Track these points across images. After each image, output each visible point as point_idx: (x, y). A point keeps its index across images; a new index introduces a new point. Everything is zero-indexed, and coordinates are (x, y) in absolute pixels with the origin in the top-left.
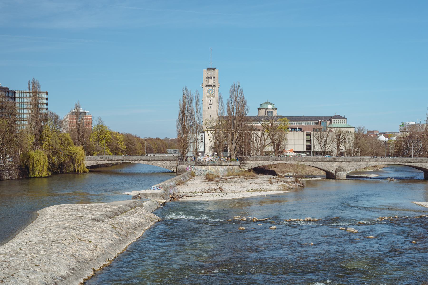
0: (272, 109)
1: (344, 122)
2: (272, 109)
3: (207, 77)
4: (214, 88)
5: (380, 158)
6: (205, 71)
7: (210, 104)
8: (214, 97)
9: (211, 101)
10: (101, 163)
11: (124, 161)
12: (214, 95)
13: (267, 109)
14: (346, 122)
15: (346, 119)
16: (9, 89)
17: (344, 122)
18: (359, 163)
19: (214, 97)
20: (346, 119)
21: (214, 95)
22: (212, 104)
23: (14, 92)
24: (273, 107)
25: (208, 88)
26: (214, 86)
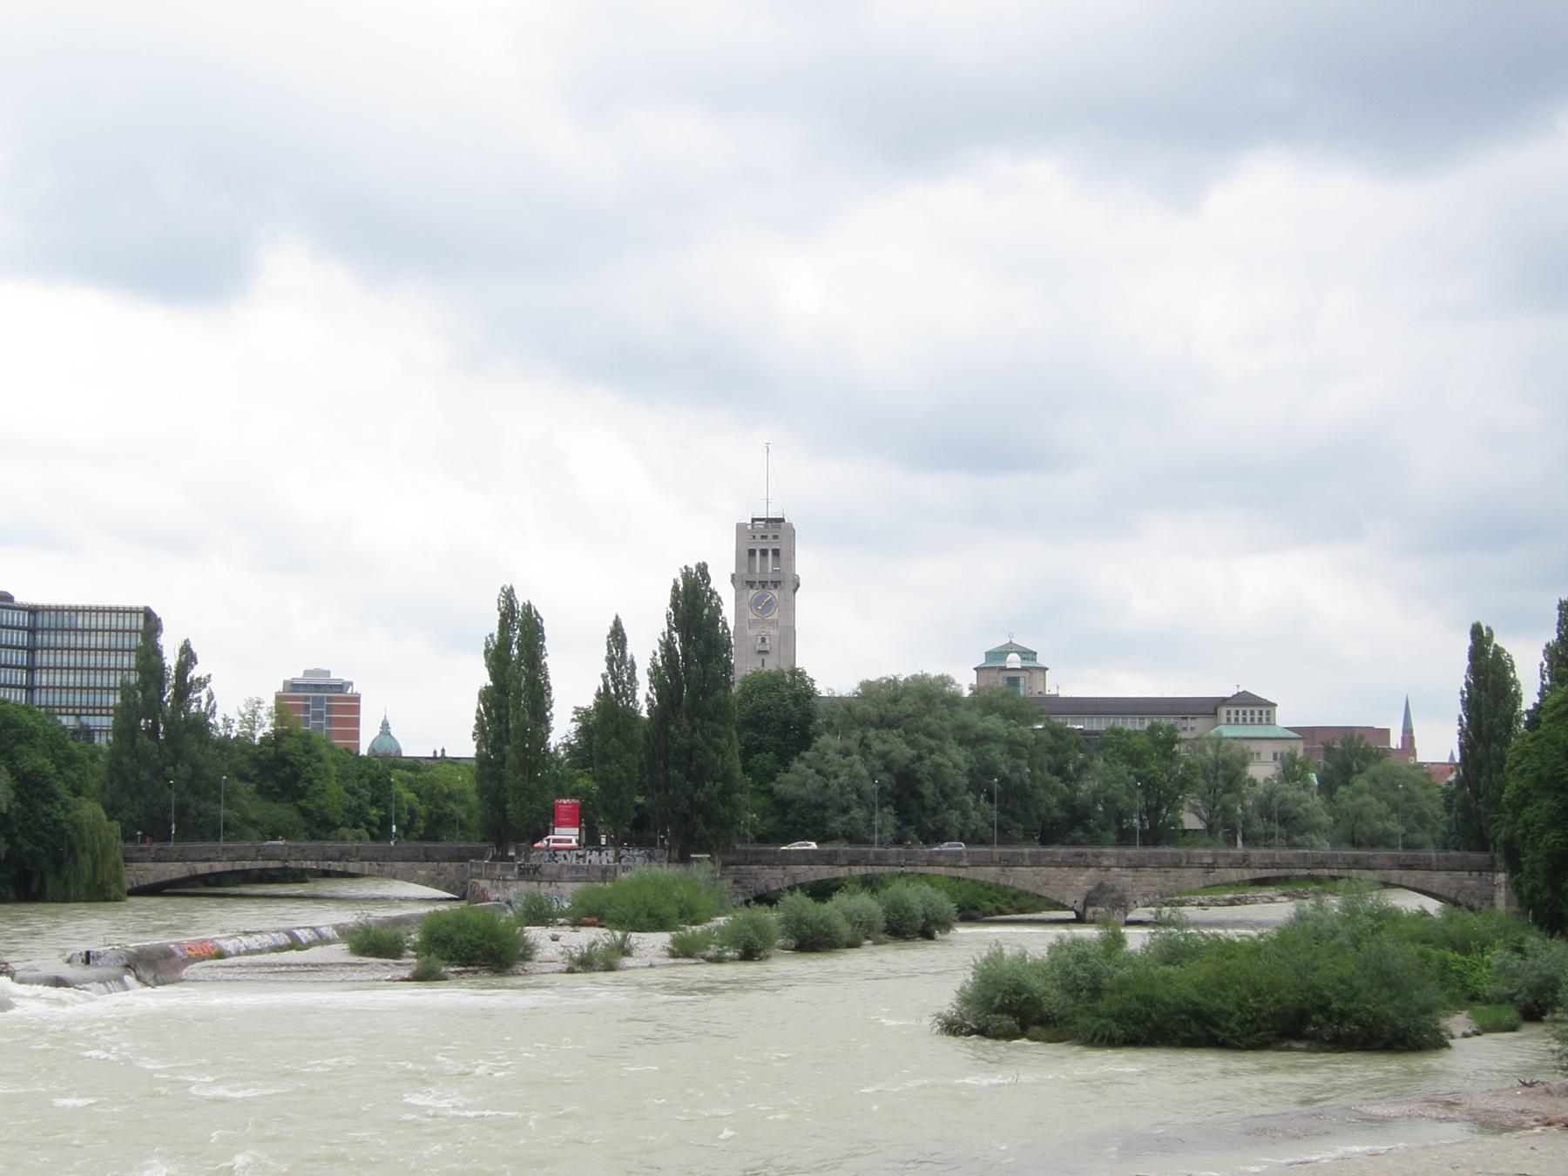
3: (752, 553)
9: (763, 640)
12: (775, 616)
13: (1004, 669)
18: (1174, 873)
21: (775, 616)
22: (760, 652)
24: (1031, 664)
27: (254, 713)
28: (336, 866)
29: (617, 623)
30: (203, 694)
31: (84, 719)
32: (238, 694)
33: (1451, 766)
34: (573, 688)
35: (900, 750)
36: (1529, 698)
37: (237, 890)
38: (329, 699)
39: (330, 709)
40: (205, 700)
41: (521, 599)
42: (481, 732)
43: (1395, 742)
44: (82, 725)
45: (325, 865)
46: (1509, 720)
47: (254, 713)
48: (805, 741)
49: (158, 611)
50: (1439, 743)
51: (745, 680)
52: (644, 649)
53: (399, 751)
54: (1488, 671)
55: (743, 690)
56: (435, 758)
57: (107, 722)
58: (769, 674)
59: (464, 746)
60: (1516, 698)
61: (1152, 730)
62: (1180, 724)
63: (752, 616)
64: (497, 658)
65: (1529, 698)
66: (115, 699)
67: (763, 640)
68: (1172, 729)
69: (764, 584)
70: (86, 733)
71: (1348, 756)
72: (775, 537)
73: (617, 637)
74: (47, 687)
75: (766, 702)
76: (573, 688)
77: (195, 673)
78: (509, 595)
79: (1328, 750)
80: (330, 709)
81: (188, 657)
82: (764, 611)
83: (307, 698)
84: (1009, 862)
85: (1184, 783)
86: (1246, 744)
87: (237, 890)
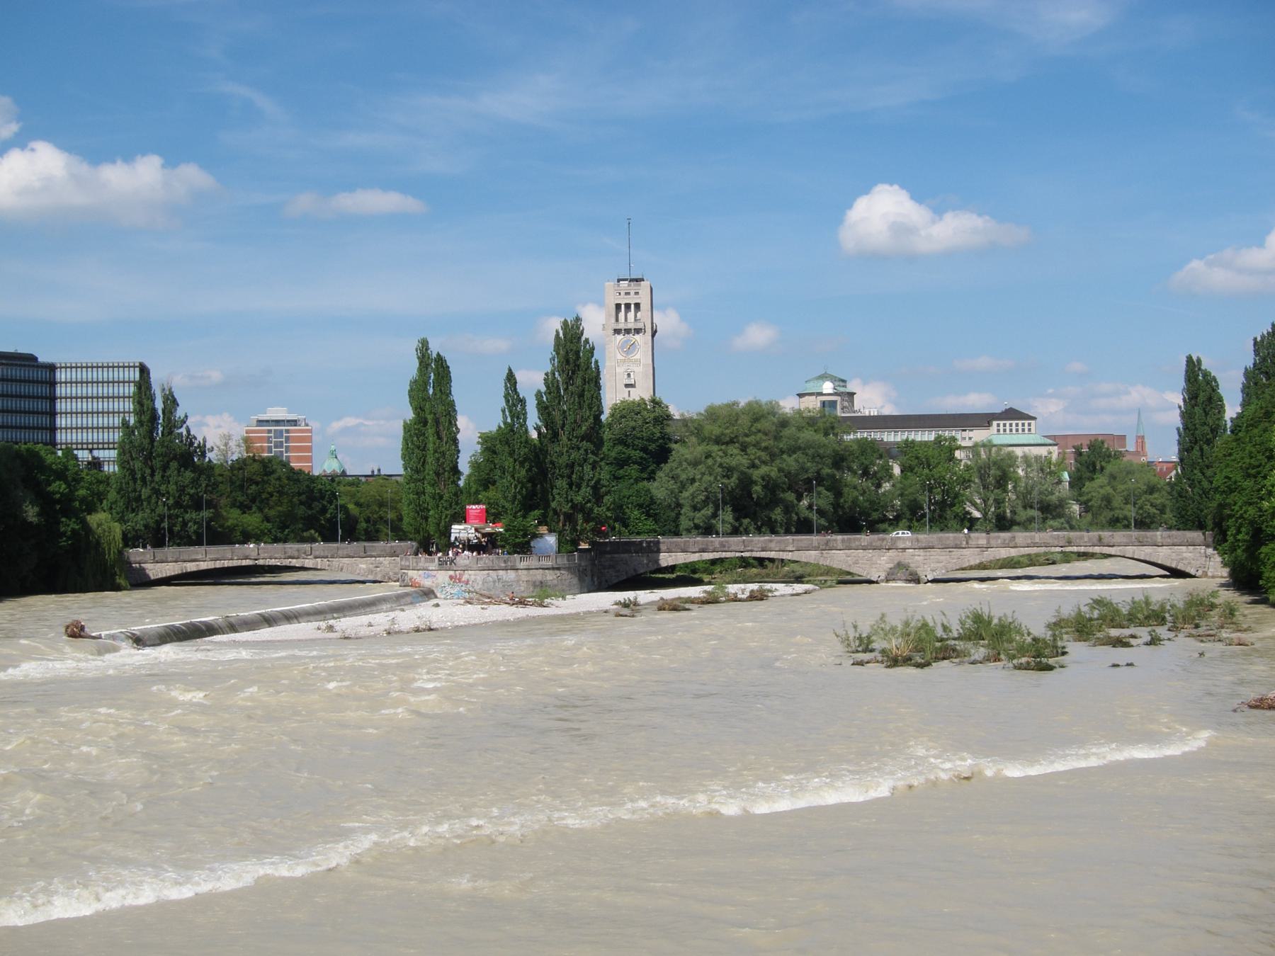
0: (835, 394)
1: (1026, 427)
2: (835, 394)
3: (618, 306)
4: (637, 337)
5: (1159, 535)
6: (610, 285)
7: (627, 386)
8: (638, 362)
9: (629, 375)
10: (194, 569)
11: (261, 562)
12: (637, 357)
13: (821, 394)
14: (1033, 427)
15: (1034, 418)
16: (40, 360)
17: (1026, 427)
18: (956, 552)
19: (638, 362)
20: (1034, 418)
21: (637, 357)
22: (627, 386)
23: (52, 368)
24: (842, 389)
25: (620, 337)
26: (638, 331)
27: (226, 445)
28: (295, 563)
29: (510, 370)
30: (183, 430)
31: (96, 453)
32: (219, 432)
33: (1175, 465)
34: (476, 421)
35: (737, 459)
36: (1232, 409)
37: (253, 580)
38: (287, 431)
39: (288, 439)
40: (185, 433)
41: (434, 349)
42: (407, 454)
43: (1131, 446)
44: (94, 458)
45: (286, 562)
46: (1216, 429)
47: (226, 445)
48: (662, 455)
49: (148, 365)
50: (1162, 448)
51: (615, 408)
52: (532, 382)
53: (163, 166)
54: (1200, 391)
55: (612, 415)
56: (372, 476)
57: (113, 454)
58: (633, 402)
59: (394, 465)
60: (1221, 409)
61: (938, 440)
62: (958, 434)
63: (619, 357)
64: (417, 392)
65: (1232, 409)
66: (117, 436)
67: (629, 375)
68: (954, 439)
69: (628, 331)
70: (96, 464)
71: (1094, 458)
72: (637, 293)
73: (511, 378)
74: (66, 428)
75: (632, 424)
76: (476, 421)
77: (180, 413)
78: (424, 344)
79: (1079, 453)
80: (288, 439)
81: (171, 401)
82: (628, 352)
83: (269, 431)
84: (828, 547)
85: (966, 482)
86: (1010, 449)
87: (253, 580)
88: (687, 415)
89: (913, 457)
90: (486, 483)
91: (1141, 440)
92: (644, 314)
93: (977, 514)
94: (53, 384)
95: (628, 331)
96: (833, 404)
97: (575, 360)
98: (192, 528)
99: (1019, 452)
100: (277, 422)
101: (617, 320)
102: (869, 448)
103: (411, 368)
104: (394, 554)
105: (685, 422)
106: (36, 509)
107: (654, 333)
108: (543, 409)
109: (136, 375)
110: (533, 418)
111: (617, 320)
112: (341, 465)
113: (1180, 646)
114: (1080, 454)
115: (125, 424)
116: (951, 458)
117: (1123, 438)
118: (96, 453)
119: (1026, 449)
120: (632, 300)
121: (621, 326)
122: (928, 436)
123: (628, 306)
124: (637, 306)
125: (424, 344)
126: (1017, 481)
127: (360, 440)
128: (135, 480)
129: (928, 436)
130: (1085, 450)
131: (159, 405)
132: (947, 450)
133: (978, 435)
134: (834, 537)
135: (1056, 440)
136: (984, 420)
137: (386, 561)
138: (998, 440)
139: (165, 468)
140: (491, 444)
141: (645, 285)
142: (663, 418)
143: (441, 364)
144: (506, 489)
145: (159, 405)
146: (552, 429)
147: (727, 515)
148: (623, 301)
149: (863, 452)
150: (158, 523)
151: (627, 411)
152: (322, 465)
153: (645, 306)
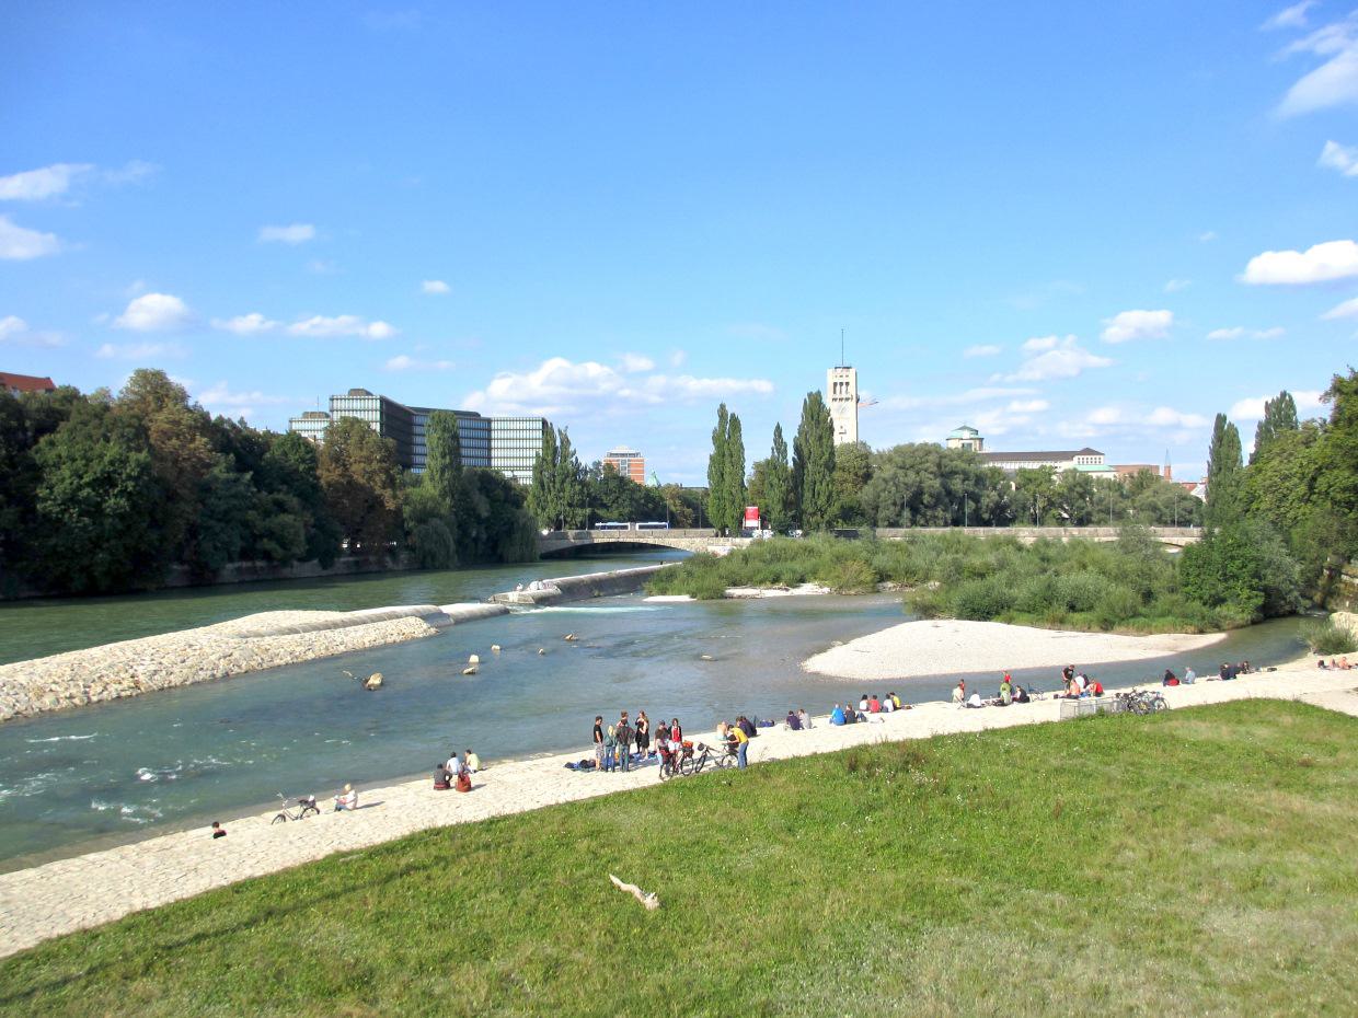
3: (835, 384)
6: (830, 372)
23: (489, 421)
26: (847, 399)
34: (756, 450)
41: (730, 410)
48: (868, 476)
54: (1225, 437)
64: (717, 438)
65: (1248, 447)
66: (532, 462)
69: (841, 399)
73: (778, 430)
76: (756, 450)
77: (571, 449)
78: (722, 407)
81: (566, 442)
88: (881, 450)
89: (1027, 479)
90: (761, 493)
91: (1168, 468)
92: (852, 388)
93: (1065, 515)
94: (489, 430)
95: (841, 399)
96: (970, 445)
97: (816, 414)
98: (579, 519)
99: (1094, 475)
100: (623, 455)
101: (835, 392)
102: (995, 471)
103: (715, 422)
104: (702, 536)
105: (881, 455)
106: (143, 549)
107: (858, 400)
108: (798, 449)
109: (539, 425)
110: (791, 454)
111: (835, 392)
112: (658, 482)
113: (1027, 614)
114: (1132, 477)
115: (537, 454)
116: (1050, 480)
117: (1157, 467)
118: (515, 473)
119: (1099, 474)
120: (844, 380)
121: (838, 396)
122: (1035, 465)
123: (841, 384)
124: (847, 384)
125: (722, 407)
126: (1092, 494)
127: (680, 465)
128: (543, 490)
129: (1035, 465)
130: (1136, 475)
131: (558, 443)
132: (1047, 474)
133: (1064, 466)
134: (977, 529)
135: (1117, 468)
136: (1068, 456)
137: (698, 540)
138: (1081, 468)
139: (563, 482)
140: (765, 470)
141: (852, 371)
142: (866, 456)
143: (735, 422)
144: (774, 498)
145: (558, 443)
146: (800, 463)
147: (907, 513)
148: (838, 380)
149: (993, 475)
150: (558, 516)
151: (847, 448)
152: (650, 482)
153: (852, 384)
